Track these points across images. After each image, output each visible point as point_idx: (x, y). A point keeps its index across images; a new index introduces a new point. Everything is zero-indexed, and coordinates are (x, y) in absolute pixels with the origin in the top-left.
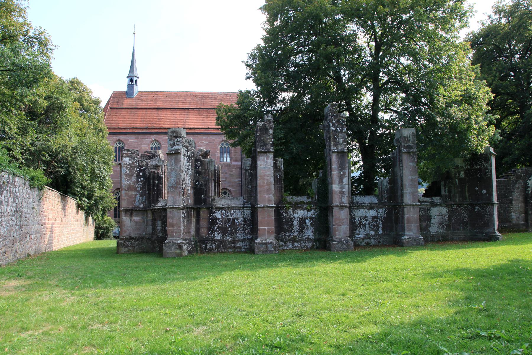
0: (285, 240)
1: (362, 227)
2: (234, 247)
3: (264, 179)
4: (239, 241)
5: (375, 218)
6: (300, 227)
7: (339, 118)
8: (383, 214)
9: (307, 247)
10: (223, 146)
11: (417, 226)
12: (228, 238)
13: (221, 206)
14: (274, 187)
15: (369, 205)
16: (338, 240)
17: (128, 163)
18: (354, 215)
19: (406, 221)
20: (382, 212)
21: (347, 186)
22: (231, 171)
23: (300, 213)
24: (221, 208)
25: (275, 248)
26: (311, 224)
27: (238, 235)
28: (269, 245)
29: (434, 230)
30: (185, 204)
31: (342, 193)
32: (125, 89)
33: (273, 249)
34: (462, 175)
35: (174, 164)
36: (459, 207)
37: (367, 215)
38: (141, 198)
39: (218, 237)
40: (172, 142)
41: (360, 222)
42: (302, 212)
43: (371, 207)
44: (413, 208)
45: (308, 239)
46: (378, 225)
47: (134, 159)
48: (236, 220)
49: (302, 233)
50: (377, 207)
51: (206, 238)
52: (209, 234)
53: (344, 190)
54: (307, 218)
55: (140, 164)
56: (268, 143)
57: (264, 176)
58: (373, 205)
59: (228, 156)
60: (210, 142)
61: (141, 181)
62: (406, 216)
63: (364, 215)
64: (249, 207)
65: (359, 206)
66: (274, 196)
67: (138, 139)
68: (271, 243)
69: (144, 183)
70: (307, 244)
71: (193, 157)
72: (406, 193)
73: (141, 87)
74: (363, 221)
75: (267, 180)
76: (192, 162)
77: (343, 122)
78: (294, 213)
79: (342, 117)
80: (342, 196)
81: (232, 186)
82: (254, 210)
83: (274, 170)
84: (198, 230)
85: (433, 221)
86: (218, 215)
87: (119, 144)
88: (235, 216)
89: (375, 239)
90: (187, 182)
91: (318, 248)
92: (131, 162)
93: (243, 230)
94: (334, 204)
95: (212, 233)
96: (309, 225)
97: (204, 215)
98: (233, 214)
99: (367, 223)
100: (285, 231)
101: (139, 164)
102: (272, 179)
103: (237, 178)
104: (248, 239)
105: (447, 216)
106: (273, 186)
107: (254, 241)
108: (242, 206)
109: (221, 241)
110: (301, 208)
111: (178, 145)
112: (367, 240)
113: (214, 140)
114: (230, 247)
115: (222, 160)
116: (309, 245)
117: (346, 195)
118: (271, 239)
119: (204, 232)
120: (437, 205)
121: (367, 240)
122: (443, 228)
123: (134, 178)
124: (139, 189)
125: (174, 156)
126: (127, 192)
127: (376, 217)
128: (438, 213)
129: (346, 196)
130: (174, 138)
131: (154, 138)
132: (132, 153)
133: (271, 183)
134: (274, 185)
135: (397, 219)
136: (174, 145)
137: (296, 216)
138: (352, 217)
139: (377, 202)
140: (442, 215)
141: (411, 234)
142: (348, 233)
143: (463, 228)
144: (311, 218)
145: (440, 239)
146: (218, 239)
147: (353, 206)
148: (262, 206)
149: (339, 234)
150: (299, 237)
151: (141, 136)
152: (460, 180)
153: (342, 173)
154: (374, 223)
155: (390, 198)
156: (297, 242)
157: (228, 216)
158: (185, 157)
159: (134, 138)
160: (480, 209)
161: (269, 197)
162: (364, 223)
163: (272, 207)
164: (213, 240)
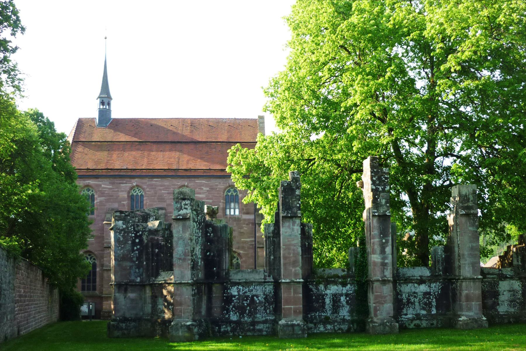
0: (315, 321)
1: (410, 305)
2: (254, 330)
3: (289, 249)
4: (259, 322)
5: (426, 294)
6: (333, 306)
7: (380, 174)
8: (436, 289)
9: (342, 329)
10: (230, 194)
11: (479, 305)
12: (246, 319)
13: (238, 281)
14: (302, 258)
15: (419, 278)
17: (121, 228)
18: (400, 291)
19: (463, 298)
20: (435, 287)
21: (390, 256)
22: (242, 228)
23: (333, 289)
24: (238, 284)
25: (303, 330)
26: (347, 302)
27: (258, 315)
28: (296, 328)
29: (503, 309)
30: (195, 279)
31: (384, 265)
32: (94, 114)
33: (300, 332)
35: (181, 232)
37: (417, 291)
38: (137, 270)
40: (179, 205)
41: (407, 299)
42: (336, 287)
43: (421, 281)
44: (474, 282)
45: (344, 320)
46: (430, 303)
47: (129, 222)
48: (255, 298)
49: (336, 312)
50: (429, 280)
51: (220, 319)
52: (223, 314)
53: (386, 261)
54: (342, 295)
55: (136, 229)
56: (294, 206)
57: (290, 245)
58: (424, 278)
59: (237, 206)
60: (212, 189)
61: (137, 250)
62: (465, 292)
63: (413, 290)
64: (272, 282)
65: (406, 280)
66: (302, 269)
67: (112, 184)
68: (298, 325)
69: (140, 251)
70: (342, 327)
71: (204, 222)
72: (465, 264)
73: (118, 112)
75: (294, 250)
76: (202, 229)
77: (386, 178)
78: (326, 288)
79: (385, 173)
80: (384, 269)
81: (243, 248)
82: (277, 285)
83: (302, 238)
84: (209, 309)
85: (502, 298)
86: (234, 291)
87: (89, 190)
88: (254, 293)
89: (426, 320)
90: (197, 253)
92: (124, 226)
93: (264, 309)
94: (375, 278)
96: (344, 303)
97: (216, 289)
98: (252, 290)
99: (417, 300)
100: (315, 310)
101: (134, 228)
102: (300, 250)
103: (249, 237)
104: (271, 320)
105: (521, 292)
106: (300, 257)
107: (278, 323)
108: (263, 280)
110: (335, 283)
111: (186, 209)
113: (217, 185)
114: (249, 330)
115: (228, 213)
116: (345, 327)
117: (390, 268)
118: (298, 321)
119: (216, 311)
122: (514, 307)
123: (128, 247)
124: (135, 259)
125: (181, 223)
126: (121, 263)
127: (429, 293)
128: (507, 288)
129: (389, 268)
130: (180, 201)
131: (135, 182)
132: (126, 216)
133: (298, 254)
134: (302, 255)
135: (454, 295)
136: (181, 209)
138: (397, 294)
139: (429, 274)
140: (513, 291)
141: (471, 314)
142: (392, 313)
144: (347, 295)
145: (511, 320)
146: (234, 320)
147: (398, 279)
148: (288, 281)
149: (381, 315)
151: (117, 181)
153: (384, 241)
154: (425, 300)
156: (330, 323)
158: (195, 223)
159: (108, 183)
161: (295, 270)
162: (412, 301)
163: (299, 282)
164: (229, 322)
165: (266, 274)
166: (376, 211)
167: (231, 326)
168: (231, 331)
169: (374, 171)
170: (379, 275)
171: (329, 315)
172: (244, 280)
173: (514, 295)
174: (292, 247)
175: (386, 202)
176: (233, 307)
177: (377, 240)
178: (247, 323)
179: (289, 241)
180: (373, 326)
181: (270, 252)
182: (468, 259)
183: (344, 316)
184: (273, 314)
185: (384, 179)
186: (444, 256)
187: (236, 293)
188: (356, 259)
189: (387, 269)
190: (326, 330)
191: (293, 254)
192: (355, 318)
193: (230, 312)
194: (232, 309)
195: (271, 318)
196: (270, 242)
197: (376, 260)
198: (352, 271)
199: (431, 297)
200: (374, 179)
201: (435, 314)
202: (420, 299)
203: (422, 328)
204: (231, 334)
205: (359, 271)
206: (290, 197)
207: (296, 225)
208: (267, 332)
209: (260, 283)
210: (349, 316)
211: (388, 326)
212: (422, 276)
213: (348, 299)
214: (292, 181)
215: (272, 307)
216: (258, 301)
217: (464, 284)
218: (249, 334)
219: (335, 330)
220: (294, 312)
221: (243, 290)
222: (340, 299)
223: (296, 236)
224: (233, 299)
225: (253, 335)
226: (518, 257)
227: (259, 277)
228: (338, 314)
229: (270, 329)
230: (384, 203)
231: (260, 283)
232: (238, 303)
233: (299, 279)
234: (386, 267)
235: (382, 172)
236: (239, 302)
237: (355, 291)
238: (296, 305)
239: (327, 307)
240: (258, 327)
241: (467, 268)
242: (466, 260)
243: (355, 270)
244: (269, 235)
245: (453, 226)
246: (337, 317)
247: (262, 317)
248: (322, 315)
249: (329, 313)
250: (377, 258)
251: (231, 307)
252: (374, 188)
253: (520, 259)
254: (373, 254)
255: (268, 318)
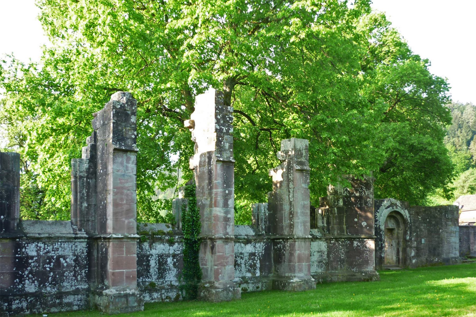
3: (122, 193)
4: (68, 294)
6: (159, 269)
7: (225, 112)
8: (260, 250)
9: (170, 298)
12: (48, 289)
13: (37, 236)
15: (246, 237)
16: (221, 286)
20: (260, 247)
23: (161, 248)
24: (38, 239)
26: (174, 264)
27: (65, 284)
31: (227, 220)
34: (341, 203)
36: (338, 242)
37: (243, 252)
39: (31, 287)
42: (162, 246)
46: (255, 265)
48: (62, 259)
51: (9, 291)
52: (14, 284)
53: (229, 216)
54: (168, 256)
56: (128, 136)
57: (123, 188)
58: (250, 238)
62: (297, 252)
63: (240, 251)
64: (85, 238)
68: (133, 295)
70: (170, 294)
72: (298, 223)
74: (238, 259)
75: (127, 195)
80: (227, 224)
86: (31, 250)
88: (60, 252)
89: (253, 283)
91: (185, 299)
93: (74, 276)
94: (217, 236)
95: (21, 282)
96: (171, 265)
98: (57, 249)
99: (243, 261)
108: (74, 236)
109: (37, 295)
110: (161, 240)
112: (244, 286)
114: (54, 305)
116: (173, 295)
120: (317, 238)
121: (244, 286)
129: (231, 224)
137: (153, 252)
140: (321, 252)
141: (301, 275)
143: (341, 267)
144: (174, 256)
149: (223, 278)
150: (158, 283)
152: (339, 208)
153: (227, 192)
154: (251, 261)
155: (268, 230)
156: (156, 291)
157: (48, 252)
160: (359, 244)
161: (129, 223)
163: (134, 238)
164: (24, 295)
165: (74, 227)
166: (219, 155)
167: (27, 300)
168: (27, 308)
169: (218, 107)
170: (222, 232)
171: (153, 281)
172: (47, 235)
173: (321, 256)
174: (125, 191)
175: (230, 147)
176: (29, 274)
177: (220, 190)
178: (51, 296)
179: (121, 183)
180: (216, 292)
181: (81, 198)
182: (300, 217)
183: (171, 281)
184: (85, 281)
185: (228, 119)
186: (267, 214)
187: (34, 254)
188: (184, 213)
189: (230, 226)
190: (152, 299)
191: (127, 200)
192: (184, 283)
193: (24, 280)
194: (28, 276)
195: (83, 287)
196: (83, 184)
197: (219, 214)
198: (178, 228)
199: (256, 258)
200: (219, 117)
201: (259, 276)
202: (246, 261)
203: (248, 292)
204: (28, 312)
205: (190, 228)
206: (123, 124)
207: (131, 162)
208: (78, 305)
209: (69, 240)
210: (176, 281)
211: (231, 291)
212: (237, 236)
213: (175, 260)
214: (127, 103)
215: (85, 272)
216: (65, 264)
217: (297, 243)
218: (53, 310)
219: (162, 299)
220: (127, 277)
221: (44, 249)
222: (167, 261)
223: (130, 176)
224: (30, 261)
225: (60, 312)
226: (323, 218)
227: (67, 231)
228: (165, 279)
229: (83, 302)
230: (227, 148)
231: (69, 240)
232: (37, 267)
233: (134, 234)
234: (228, 223)
235: (226, 111)
236: (39, 266)
237: (184, 252)
238: (129, 268)
239: (151, 270)
240: (66, 300)
241: (299, 227)
242: (299, 219)
243: (183, 226)
244: (82, 174)
245: (281, 182)
246: (163, 283)
247: (72, 286)
248: (146, 281)
249: (154, 279)
250: (220, 211)
251: (26, 273)
252: (218, 128)
253: (325, 221)
254: (216, 206)
255: (79, 287)
